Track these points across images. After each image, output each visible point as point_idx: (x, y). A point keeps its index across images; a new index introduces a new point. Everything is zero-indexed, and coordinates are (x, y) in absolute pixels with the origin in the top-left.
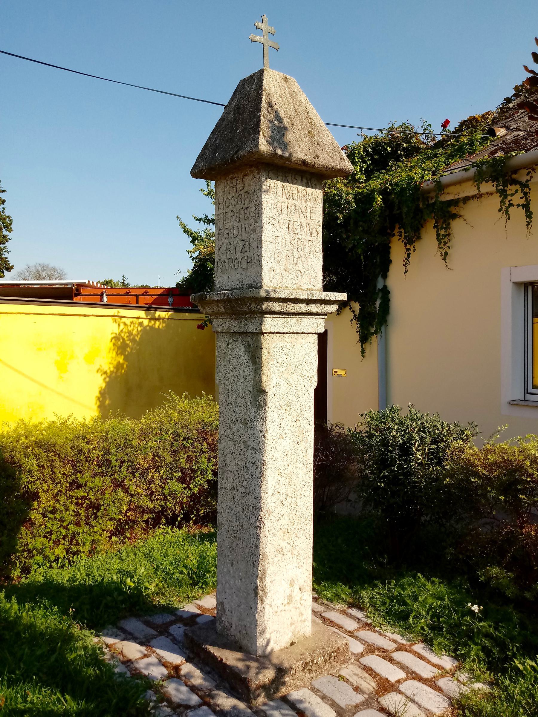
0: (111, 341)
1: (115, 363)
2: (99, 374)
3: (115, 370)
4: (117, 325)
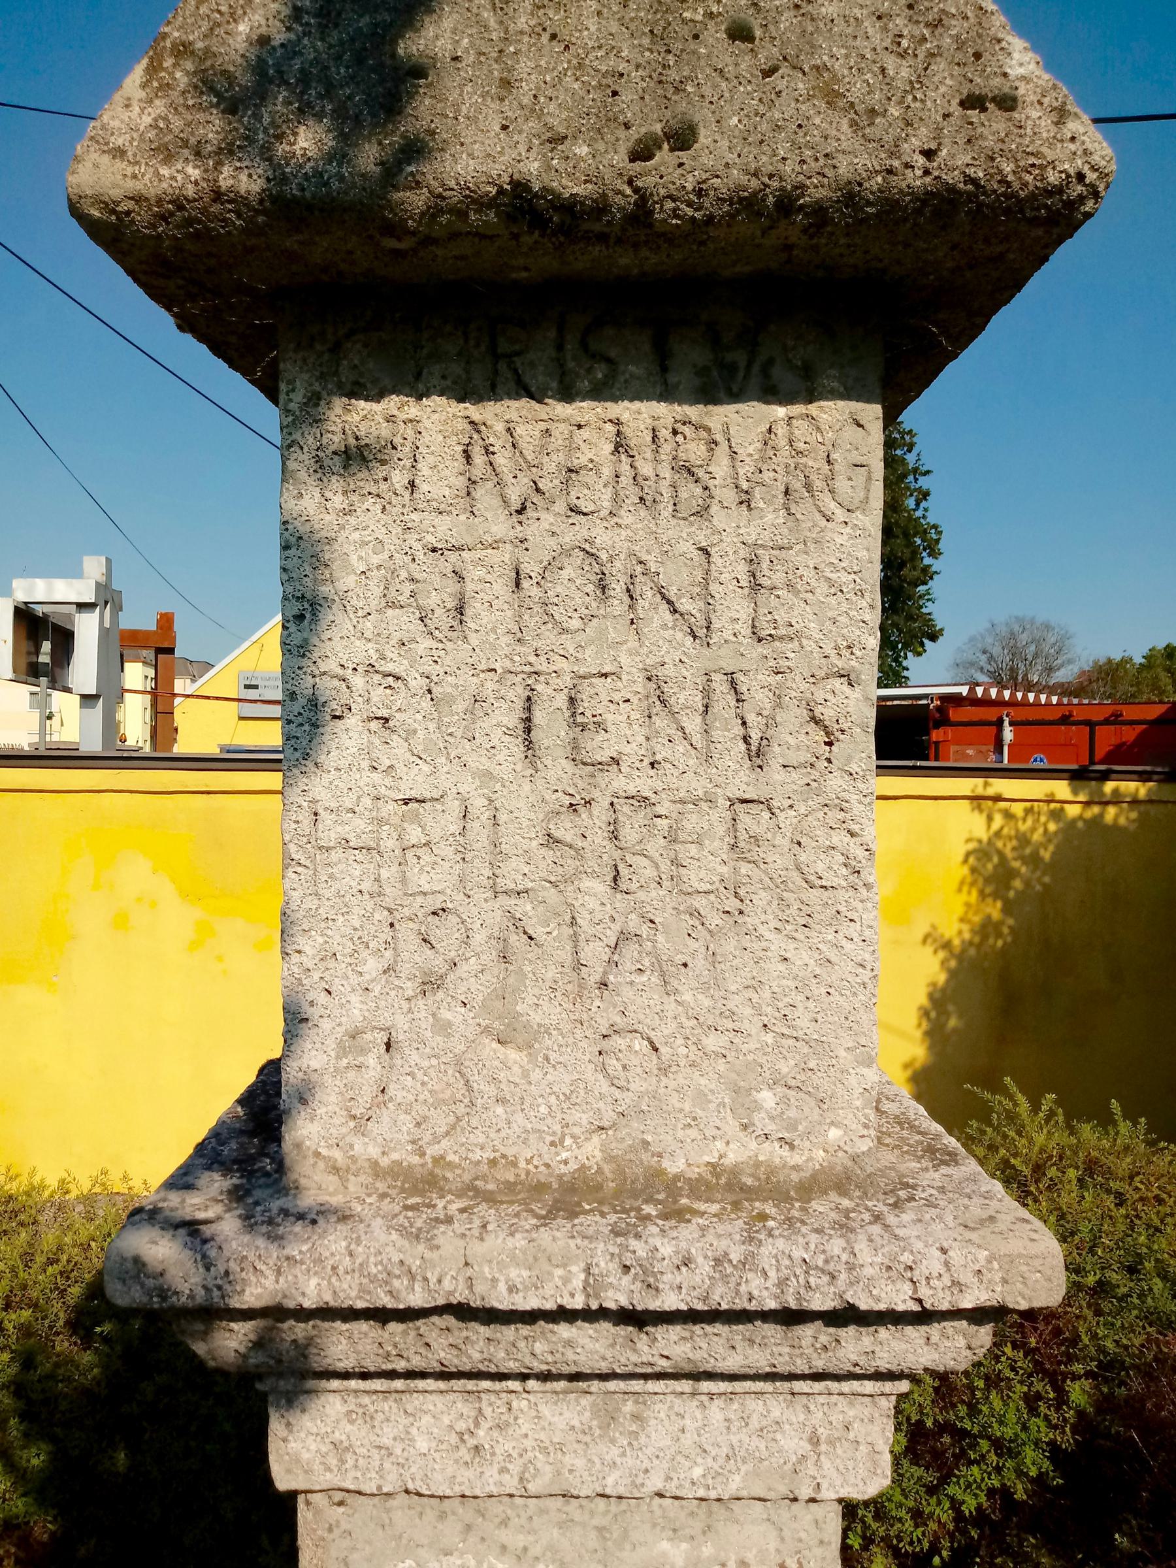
0: (965, 861)
1: (977, 919)
2: (929, 949)
3: (977, 939)
4: (984, 816)
